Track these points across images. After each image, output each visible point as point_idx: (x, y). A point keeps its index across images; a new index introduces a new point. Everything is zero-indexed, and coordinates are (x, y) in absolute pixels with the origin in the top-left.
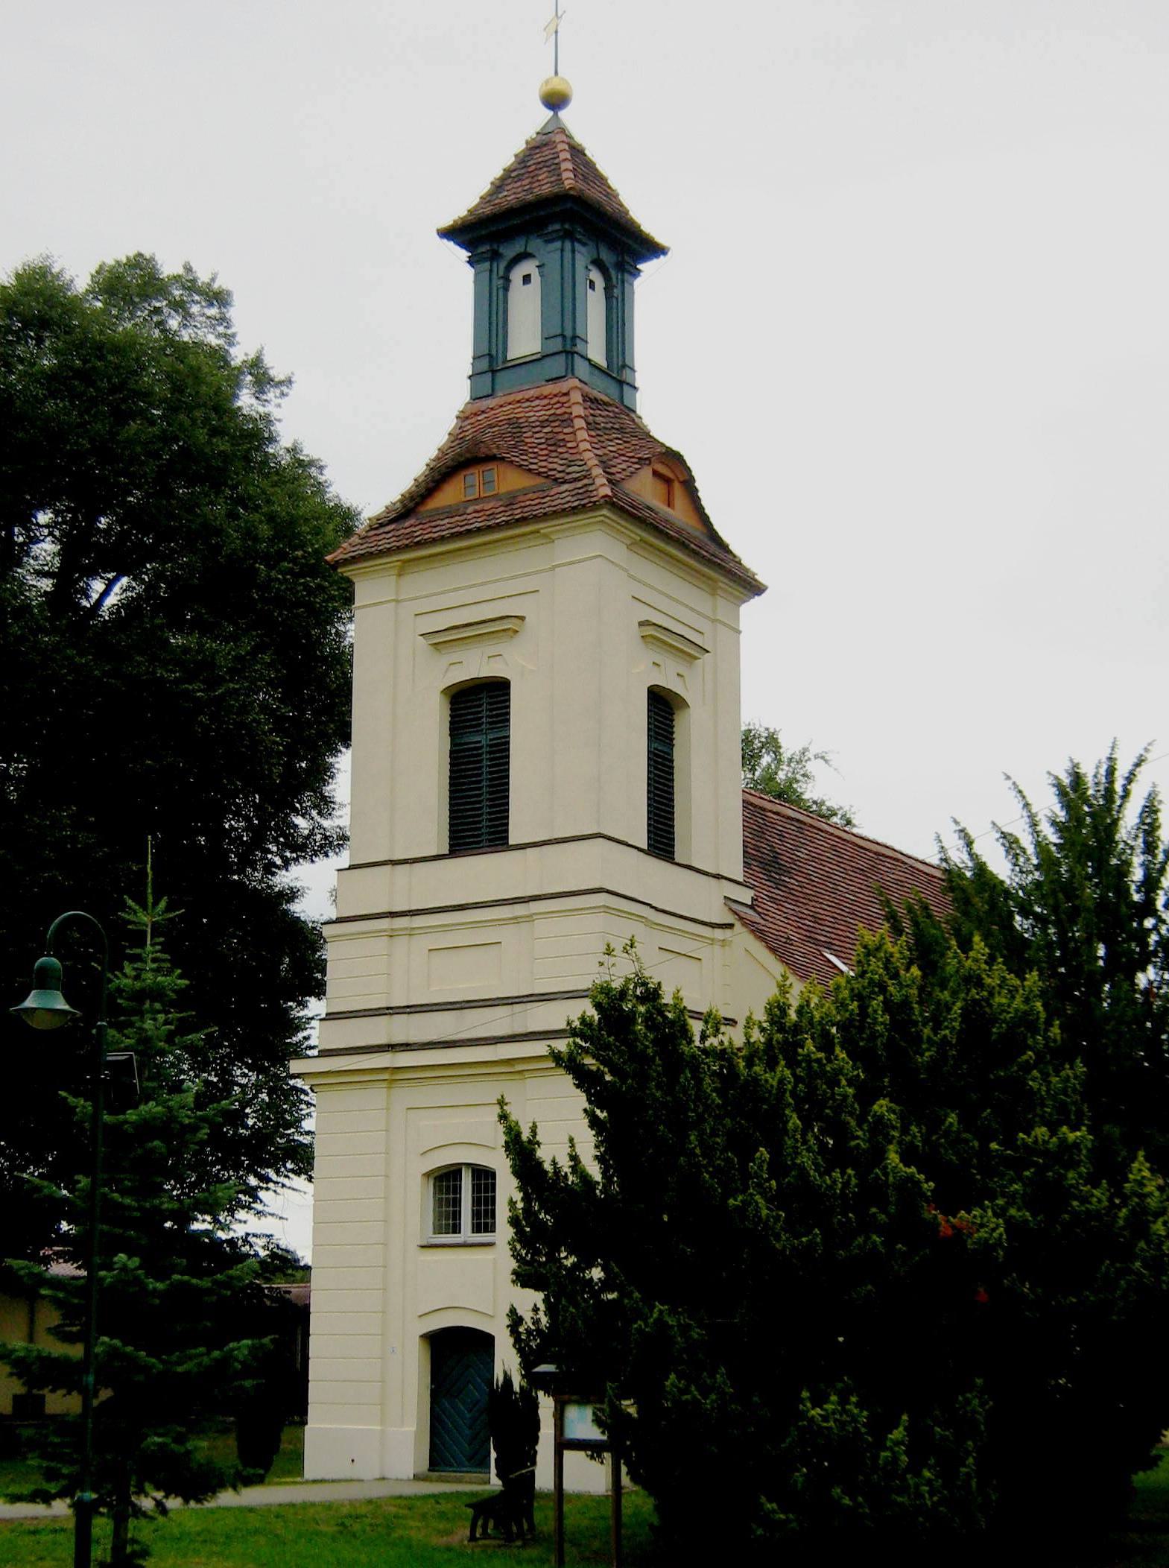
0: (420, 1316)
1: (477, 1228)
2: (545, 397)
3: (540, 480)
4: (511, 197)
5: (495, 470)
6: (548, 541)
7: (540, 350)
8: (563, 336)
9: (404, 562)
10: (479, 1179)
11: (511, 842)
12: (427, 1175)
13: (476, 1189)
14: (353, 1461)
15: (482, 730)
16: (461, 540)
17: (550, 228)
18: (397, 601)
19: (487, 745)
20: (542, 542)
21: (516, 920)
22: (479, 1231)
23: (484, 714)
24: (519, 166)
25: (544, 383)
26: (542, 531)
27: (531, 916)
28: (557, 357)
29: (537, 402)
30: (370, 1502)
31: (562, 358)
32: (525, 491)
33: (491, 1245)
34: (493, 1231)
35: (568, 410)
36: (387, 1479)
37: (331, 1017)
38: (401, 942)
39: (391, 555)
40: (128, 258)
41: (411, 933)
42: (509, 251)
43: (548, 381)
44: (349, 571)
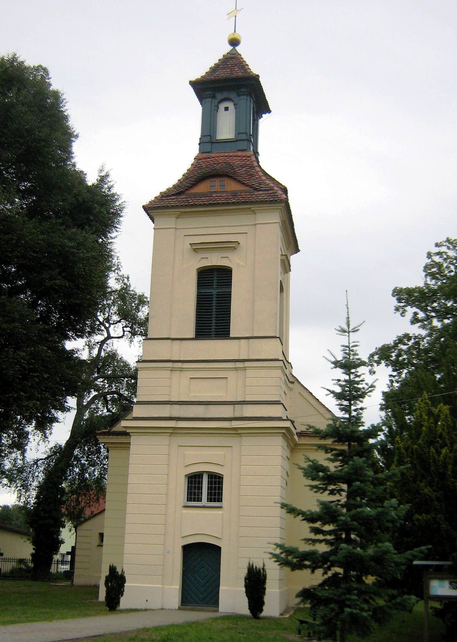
0: (182, 537)
1: (210, 500)
2: (239, 156)
3: (247, 188)
4: (222, 74)
5: (226, 181)
6: (253, 213)
7: (234, 138)
8: (210, 136)
9: (182, 212)
10: (212, 478)
11: (231, 336)
12: (186, 476)
13: (210, 483)
14: (147, 601)
15: (214, 288)
16: (233, 205)
17: (242, 90)
18: (176, 229)
19: (215, 294)
20: (251, 213)
21: (236, 369)
22: (211, 501)
23: (215, 281)
24: (221, 64)
25: (237, 151)
26: (252, 209)
27: (245, 367)
28: (207, 144)
29: (235, 158)
30: (107, 615)
31: (246, 142)
32: (241, 192)
33: (221, 507)
34: (221, 502)
35: (251, 163)
36: (164, 609)
37: (139, 403)
38: (176, 374)
39: (247, 205)
40: (23, 62)
41: (181, 370)
42: (219, 96)
43: (238, 150)
44: (152, 212)
